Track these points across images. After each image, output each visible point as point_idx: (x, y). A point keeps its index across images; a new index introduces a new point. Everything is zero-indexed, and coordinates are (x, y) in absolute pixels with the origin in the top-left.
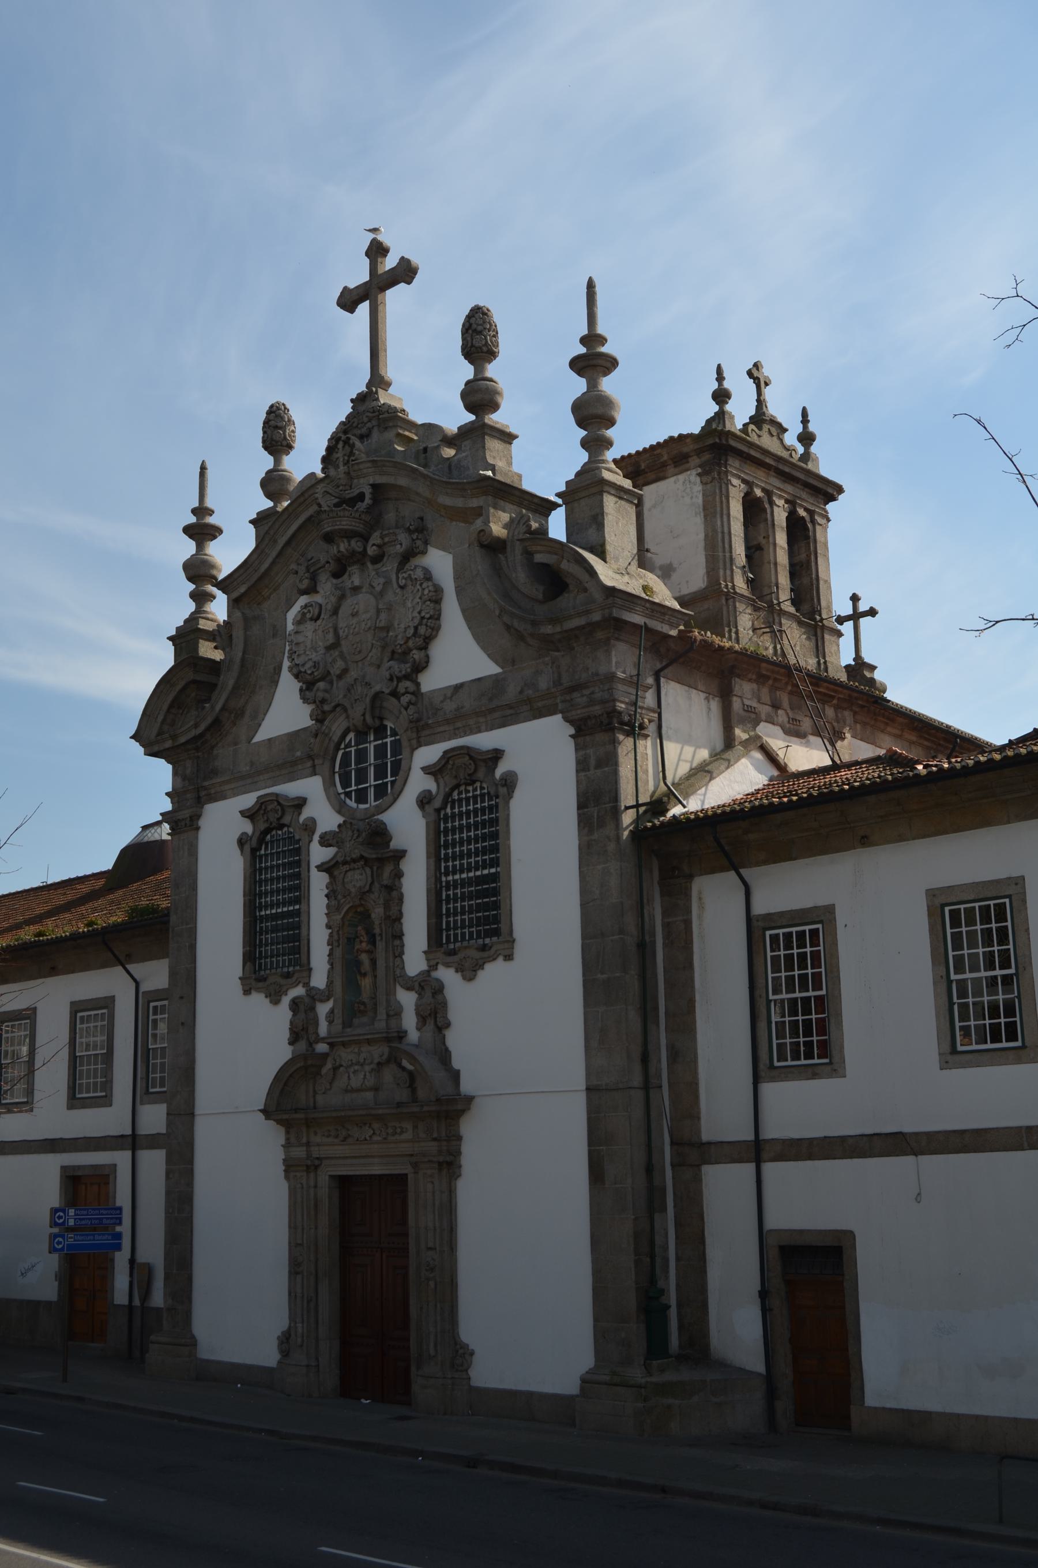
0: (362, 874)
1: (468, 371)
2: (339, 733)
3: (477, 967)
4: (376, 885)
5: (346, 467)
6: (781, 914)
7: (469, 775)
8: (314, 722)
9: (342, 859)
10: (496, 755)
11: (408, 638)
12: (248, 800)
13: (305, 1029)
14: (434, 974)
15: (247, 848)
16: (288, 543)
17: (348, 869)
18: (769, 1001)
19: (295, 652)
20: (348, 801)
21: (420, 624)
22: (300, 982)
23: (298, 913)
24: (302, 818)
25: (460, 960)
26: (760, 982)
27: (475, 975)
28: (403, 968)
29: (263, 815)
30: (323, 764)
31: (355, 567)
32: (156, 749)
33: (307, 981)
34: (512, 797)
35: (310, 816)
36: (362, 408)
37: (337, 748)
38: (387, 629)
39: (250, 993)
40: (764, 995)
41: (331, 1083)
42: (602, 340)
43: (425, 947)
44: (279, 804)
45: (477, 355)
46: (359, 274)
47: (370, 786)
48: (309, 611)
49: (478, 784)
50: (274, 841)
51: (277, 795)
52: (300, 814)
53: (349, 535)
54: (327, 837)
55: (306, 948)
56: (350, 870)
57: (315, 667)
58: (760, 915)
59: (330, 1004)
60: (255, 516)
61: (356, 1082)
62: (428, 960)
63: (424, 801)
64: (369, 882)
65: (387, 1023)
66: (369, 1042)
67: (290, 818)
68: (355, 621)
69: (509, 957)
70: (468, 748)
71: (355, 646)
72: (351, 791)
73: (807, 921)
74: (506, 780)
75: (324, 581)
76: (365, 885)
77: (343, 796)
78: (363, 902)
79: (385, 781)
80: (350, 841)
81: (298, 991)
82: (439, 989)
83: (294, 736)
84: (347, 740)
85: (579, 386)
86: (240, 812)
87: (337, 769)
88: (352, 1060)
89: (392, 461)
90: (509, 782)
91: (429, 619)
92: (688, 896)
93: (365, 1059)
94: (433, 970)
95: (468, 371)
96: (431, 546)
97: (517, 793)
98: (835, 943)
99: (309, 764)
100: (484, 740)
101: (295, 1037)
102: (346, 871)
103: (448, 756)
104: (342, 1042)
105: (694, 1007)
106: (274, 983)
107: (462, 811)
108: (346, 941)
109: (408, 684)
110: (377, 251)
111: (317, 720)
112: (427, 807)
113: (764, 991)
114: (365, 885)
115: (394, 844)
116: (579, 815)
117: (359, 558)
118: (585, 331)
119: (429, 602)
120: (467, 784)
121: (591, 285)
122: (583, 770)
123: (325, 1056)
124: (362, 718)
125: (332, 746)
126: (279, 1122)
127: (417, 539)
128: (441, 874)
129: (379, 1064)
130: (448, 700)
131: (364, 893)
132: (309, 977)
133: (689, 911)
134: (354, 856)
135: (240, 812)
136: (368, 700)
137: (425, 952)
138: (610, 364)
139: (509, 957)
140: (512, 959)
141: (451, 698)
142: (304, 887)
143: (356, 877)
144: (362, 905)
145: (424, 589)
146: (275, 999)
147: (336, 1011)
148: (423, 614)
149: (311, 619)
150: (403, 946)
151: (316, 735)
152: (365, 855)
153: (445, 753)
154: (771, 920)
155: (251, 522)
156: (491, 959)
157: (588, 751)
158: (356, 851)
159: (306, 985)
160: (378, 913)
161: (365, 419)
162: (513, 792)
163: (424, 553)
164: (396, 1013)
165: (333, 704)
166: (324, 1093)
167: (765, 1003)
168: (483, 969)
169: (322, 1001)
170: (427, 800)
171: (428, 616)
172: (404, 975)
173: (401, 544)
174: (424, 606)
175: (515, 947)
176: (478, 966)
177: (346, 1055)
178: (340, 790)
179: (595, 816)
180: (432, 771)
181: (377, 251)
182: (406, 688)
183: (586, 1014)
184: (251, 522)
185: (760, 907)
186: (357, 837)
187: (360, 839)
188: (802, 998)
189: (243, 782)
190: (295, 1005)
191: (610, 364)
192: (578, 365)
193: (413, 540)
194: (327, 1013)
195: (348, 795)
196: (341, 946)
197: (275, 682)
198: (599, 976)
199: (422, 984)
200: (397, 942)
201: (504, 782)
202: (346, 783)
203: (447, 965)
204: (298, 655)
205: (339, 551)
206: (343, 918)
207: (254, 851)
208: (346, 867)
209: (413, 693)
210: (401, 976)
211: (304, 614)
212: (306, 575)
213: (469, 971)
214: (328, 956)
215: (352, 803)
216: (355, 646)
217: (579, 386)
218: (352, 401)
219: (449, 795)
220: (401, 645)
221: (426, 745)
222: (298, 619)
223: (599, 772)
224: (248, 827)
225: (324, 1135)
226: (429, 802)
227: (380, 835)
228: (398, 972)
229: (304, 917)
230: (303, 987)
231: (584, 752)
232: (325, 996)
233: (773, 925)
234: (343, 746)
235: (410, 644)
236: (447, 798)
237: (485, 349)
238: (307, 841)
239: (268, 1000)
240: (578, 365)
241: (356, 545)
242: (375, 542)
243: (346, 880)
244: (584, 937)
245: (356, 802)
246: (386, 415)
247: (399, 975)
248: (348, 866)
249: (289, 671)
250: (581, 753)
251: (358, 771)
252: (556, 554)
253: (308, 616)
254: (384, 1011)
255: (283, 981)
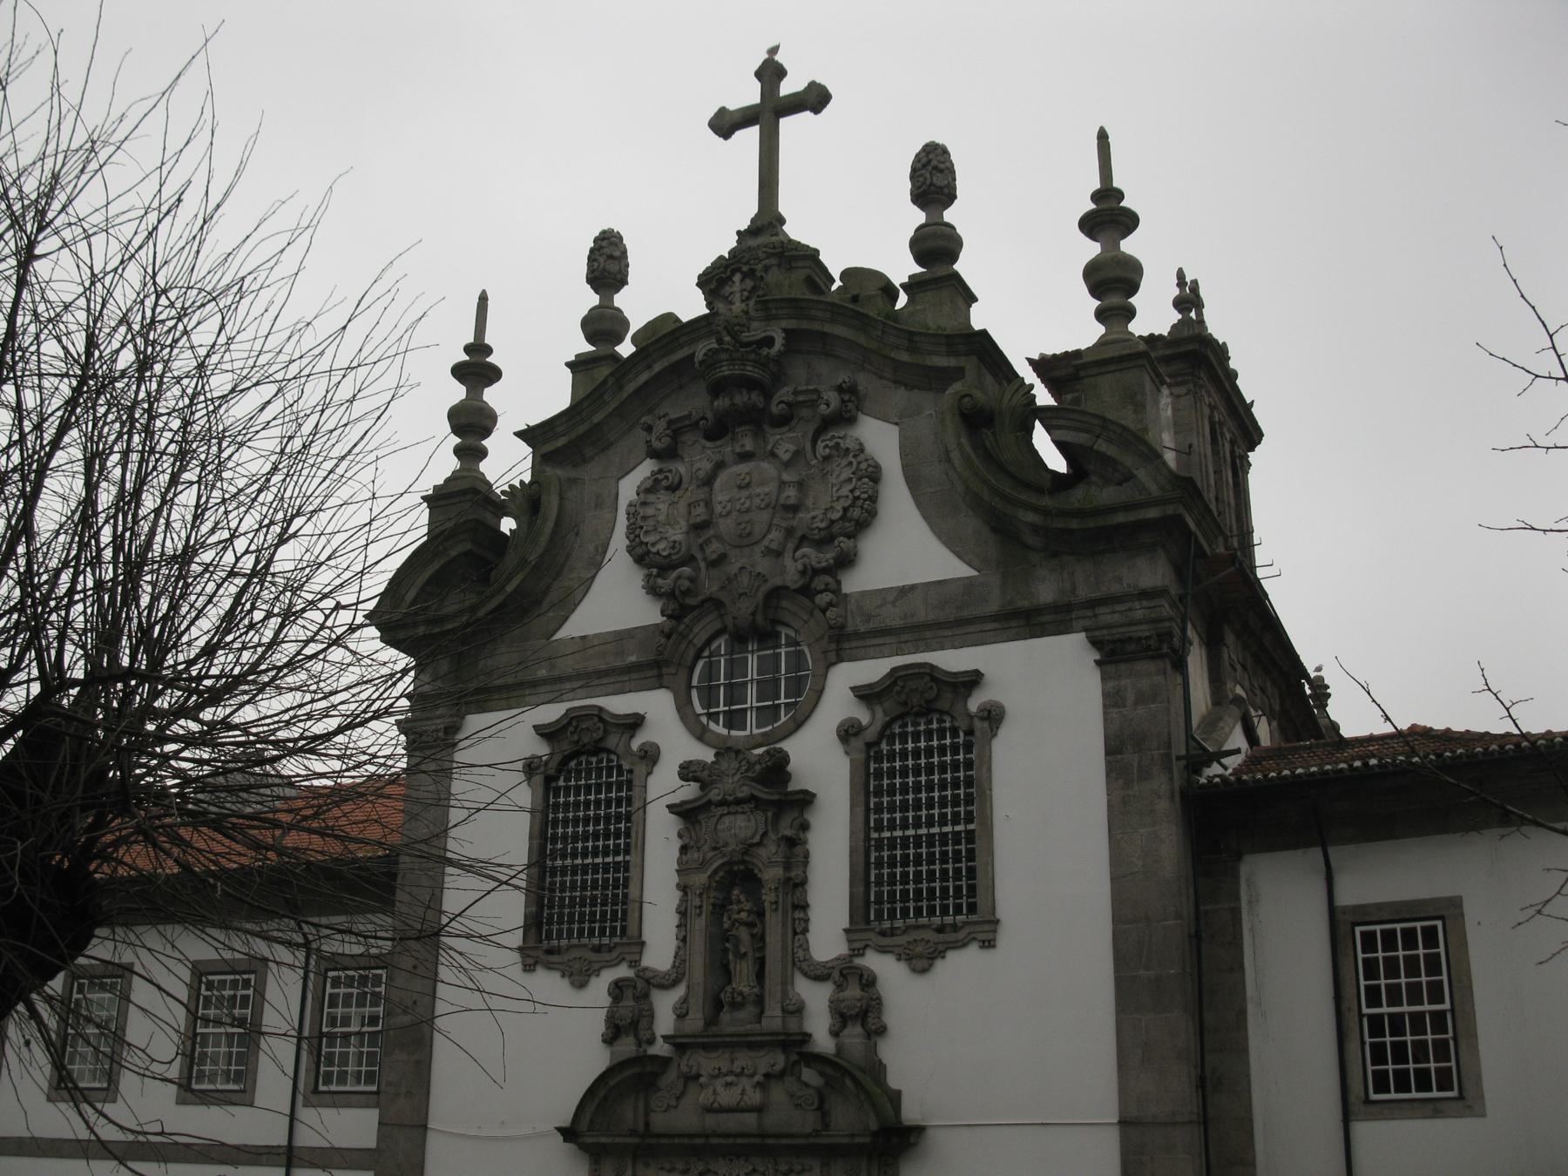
0: (749, 820)
1: (919, 217)
2: (703, 637)
3: (936, 954)
4: (772, 836)
5: (744, 305)
6: (1379, 907)
7: (928, 702)
8: (665, 618)
9: (719, 798)
10: (973, 680)
11: (832, 522)
12: (551, 713)
13: (634, 1025)
14: (858, 961)
15: (858, 743)
16: (637, 392)
17: (725, 812)
18: (1361, 1015)
19: (641, 527)
20: (712, 726)
21: (852, 505)
22: (624, 959)
23: (626, 866)
24: (635, 745)
25: (908, 942)
26: (1349, 992)
27: (931, 965)
28: (807, 949)
29: (573, 733)
30: (676, 674)
31: (747, 427)
32: (402, 635)
33: (637, 958)
34: (995, 735)
35: (652, 740)
36: (753, 242)
37: (698, 656)
38: (794, 509)
39: (534, 970)
40: (1355, 1007)
41: (678, 1098)
42: (488, 350)
43: (846, 924)
44: (601, 719)
45: (936, 196)
46: (749, 94)
47: (752, 708)
48: (667, 478)
49: (935, 717)
50: (601, 769)
51: (600, 709)
52: (632, 736)
53: (750, 384)
54: (693, 768)
55: (637, 915)
56: (729, 813)
57: (673, 547)
58: (1347, 906)
59: (679, 992)
60: (907, 280)
61: (727, 1097)
62: (850, 941)
63: (848, 732)
64: (761, 832)
65: (783, 1022)
66: (752, 1046)
67: (616, 741)
68: (745, 493)
69: (989, 944)
70: (932, 667)
71: (743, 526)
72: (718, 713)
73: (1418, 916)
74: (990, 712)
75: (690, 443)
76: (754, 835)
77: (704, 719)
78: (747, 858)
79: (776, 702)
80: (734, 774)
81: (623, 971)
82: (868, 981)
83: (621, 638)
84: (714, 646)
85: (458, 392)
86: (534, 726)
87: (695, 682)
88: (719, 1069)
89: (822, 302)
90: (994, 716)
91: (865, 500)
92: (1236, 877)
93: (743, 1068)
94: (857, 955)
95: (919, 217)
96: (863, 413)
97: (1003, 732)
98: (1464, 944)
99: (655, 672)
100: (953, 660)
101: (614, 1032)
102: (722, 815)
103: (896, 677)
104: (704, 1043)
105: (1245, 1020)
106: (580, 958)
107: (895, 750)
108: (711, 908)
109: (828, 579)
110: (771, 72)
111: (670, 617)
112: (853, 740)
113: (1356, 1002)
114: (754, 835)
115: (793, 786)
116: (1108, 763)
117: (757, 420)
118: (1097, 185)
119: (866, 480)
120: (918, 715)
121: (483, 299)
122: (1115, 705)
123: (664, 1062)
124: (751, 618)
125: (692, 652)
126: (584, 1148)
127: (850, 401)
128: (869, 828)
129: (767, 1076)
130: (889, 606)
131: (752, 845)
132: (641, 953)
133: (1237, 898)
134: (740, 795)
135: (534, 726)
136: (760, 595)
137: (846, 931)
138: (493, 374)
139: (989, 944)
140: (994, 946)
141: (894, 603)
142: (637, 833)
143: (738, 823)
144: (743, 862)
145: (859, 463)
146: (580, 979)
147: (692, 1001)
148: (857, 493)
149: (667, 488)
150: (807, 921)
151: (668, 636)
152: (756, 793)
153: (894, 670)
154: (1363, 914)
155: (568, 365)
156: (960, 944)
157: (1123, 682)
158: (745, 788)
159: (634, 964)
160: (771, 875)
161: (761, 255)
162: (998, 728)
163: (852, 421)
164: (798, 1010)
165: (700, 598)
166: (665, 1111)
167: (1357, 1018)
168: (943, 957)
169: (663, 987)
170: (854, 730)
171: (866, 496)
172: (808, 958)
173: (828, 405)
174: (859, 483)
175: (998, 931)
176: (937, 953)
177: (706, 1063)
178: (699, 709)
179: (1136, 765)
180: (866, 695)
181: (771, 72)
182: (827, 584)
183: (1119, 1022)
184: (568, 365)
185: (1345, 897)
186: (747, 771)
187: (750, 774)
188: (1410, 1014)
189: (553, 686)
190: (618, 989)
191: (493, 374)
192: (1089, 225)
193: (843, 401)
194: (676, 1003)
195: (713, 717)
196: (704, 917)
197: (596, 565)
198: (1142, 972)
199: (844, 972)
200: (799, 915)
201: (986, 714)
202: (709, 699)
203: (883, 950)
204: (646, 532)
205: (733, 404)
206: (710, 877)
207: (549, 780)
208: (720, 811)
209: (833, 592)
210: (805, 960)
211: (656, 481)
212: (667, 432)
213: (922, 961)
214: (677, 927)
215: (719, 729)
216: (743, 526)
217: (458, 392)
218: (739, 233)
219: (887, 725)
220: (820, 529)
221: (849, 660)
222: (648, 486)
223: (1140, 711)
224: (542, 749)
225: (662, 1169)
226: (856, 734)
227: (777, 768)
228: (800, 954)
229: (633, 873)
230: (630, 966)
231: (1117, 683)
232: (668, 983)
233: (1368, 919)
234: (706, 653)
235: (836, 528)
236: (885, 733)
237: (946, 191)
238: (645, 772)
239: (566, 982)
240: (1089, 225)
241: (756, 398)
242: (785, 399)
243: (719, 827)
244: (1116, 920)
245: (724, 726)
246: (794, 253)
247: (802, 959)
248: (726, 808)
249: (629, 552)
250: (1111, 684)
251: (730, 687)
252: (1087, 431)
253: (664, 483)
254: (779, 1005)
255: (593, 956)
